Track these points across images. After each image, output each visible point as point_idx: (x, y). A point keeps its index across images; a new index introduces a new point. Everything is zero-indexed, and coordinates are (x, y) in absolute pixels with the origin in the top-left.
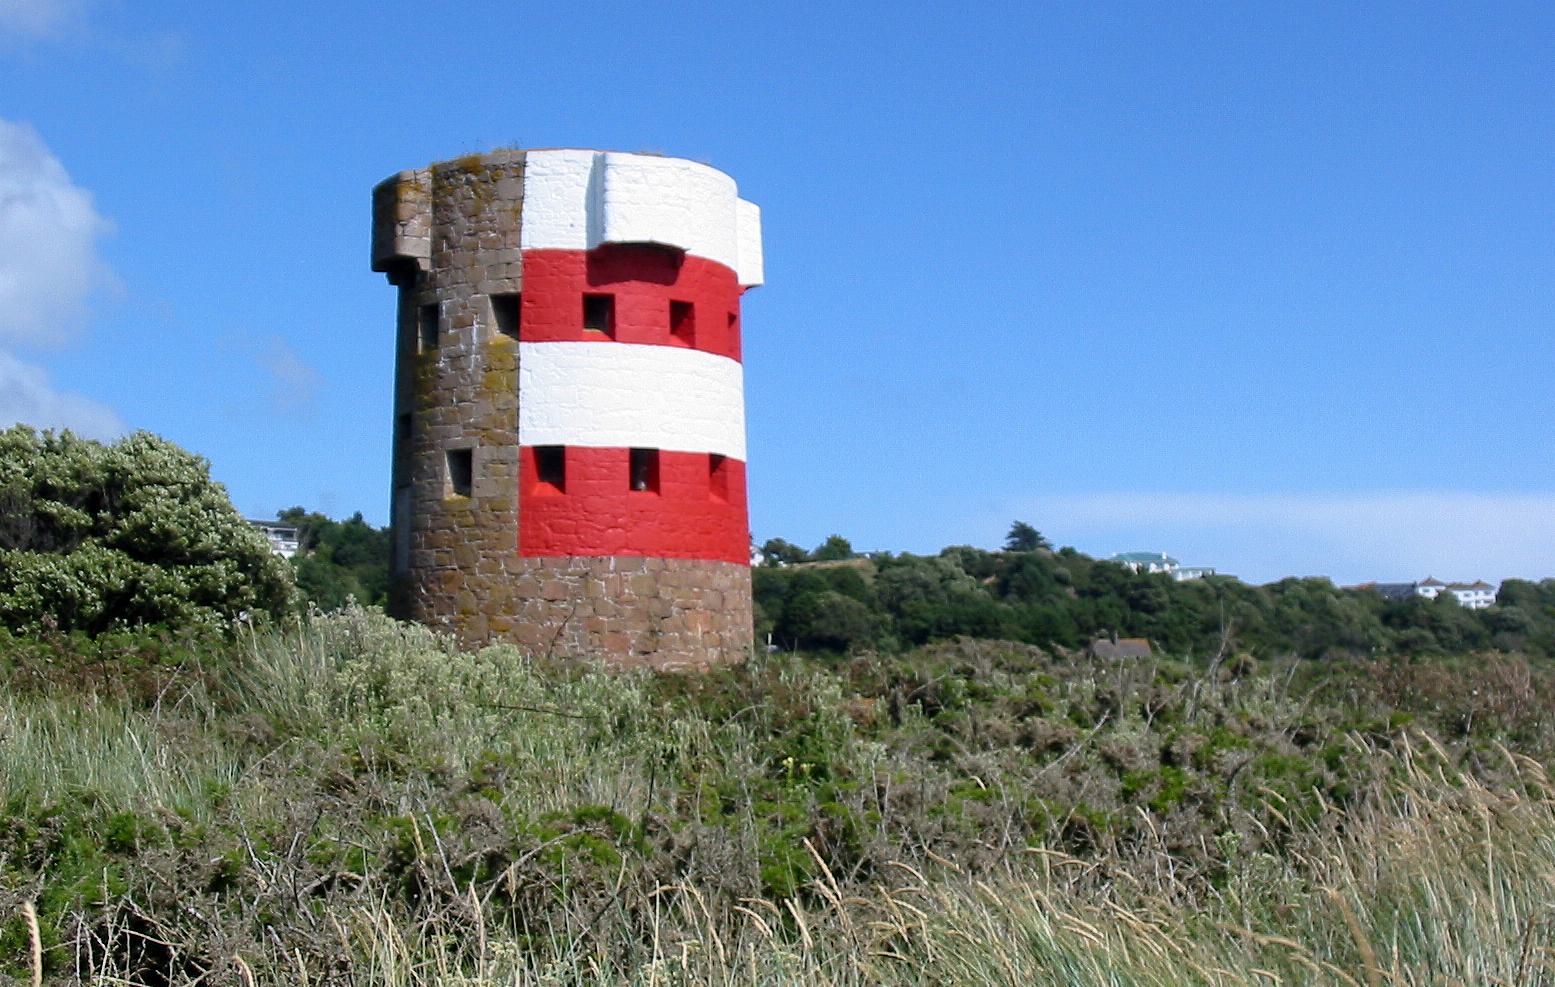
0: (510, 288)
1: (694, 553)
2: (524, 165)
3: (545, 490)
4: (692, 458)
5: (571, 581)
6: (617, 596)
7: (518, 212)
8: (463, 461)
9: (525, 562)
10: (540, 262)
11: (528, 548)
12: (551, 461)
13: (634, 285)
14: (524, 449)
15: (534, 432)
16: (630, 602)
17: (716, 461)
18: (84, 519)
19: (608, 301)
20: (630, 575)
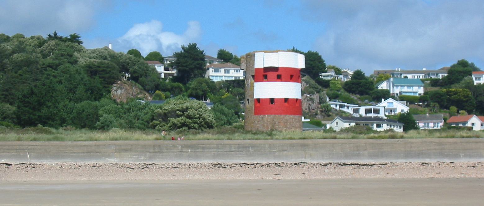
0: (253, 74)
1: (281, 114)
2: (255, 55)
3: (258, 105)
4: (266, 99)
5: (261, 119)
6: (267, 121)
7: (254, 62)
8: (248, 100)
9: (255, 116)
10: (257, 70)
11: (256, 113)
12: (258, 100)
13: (269, 72)
14: (255, 99)
15: (256, 97)
16: (269, 122)
17: (297, 99)
18: (181, 113)
19: (266, 75)
20: (269, 118)
